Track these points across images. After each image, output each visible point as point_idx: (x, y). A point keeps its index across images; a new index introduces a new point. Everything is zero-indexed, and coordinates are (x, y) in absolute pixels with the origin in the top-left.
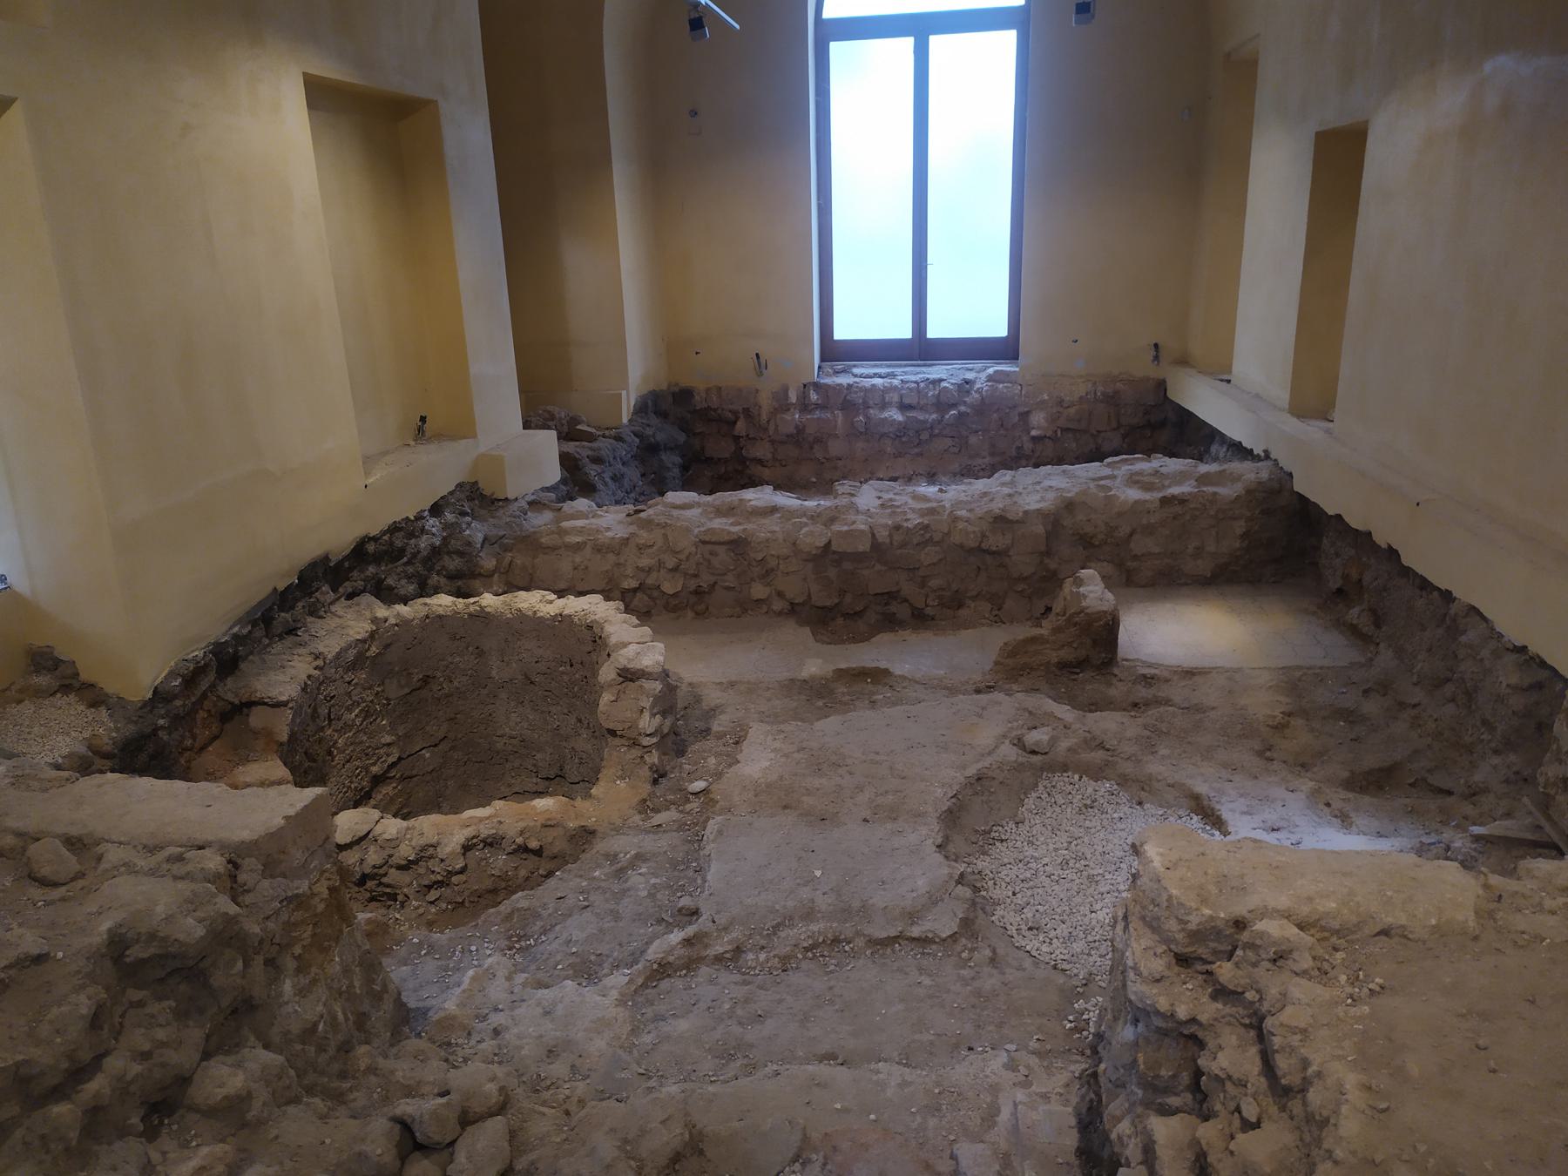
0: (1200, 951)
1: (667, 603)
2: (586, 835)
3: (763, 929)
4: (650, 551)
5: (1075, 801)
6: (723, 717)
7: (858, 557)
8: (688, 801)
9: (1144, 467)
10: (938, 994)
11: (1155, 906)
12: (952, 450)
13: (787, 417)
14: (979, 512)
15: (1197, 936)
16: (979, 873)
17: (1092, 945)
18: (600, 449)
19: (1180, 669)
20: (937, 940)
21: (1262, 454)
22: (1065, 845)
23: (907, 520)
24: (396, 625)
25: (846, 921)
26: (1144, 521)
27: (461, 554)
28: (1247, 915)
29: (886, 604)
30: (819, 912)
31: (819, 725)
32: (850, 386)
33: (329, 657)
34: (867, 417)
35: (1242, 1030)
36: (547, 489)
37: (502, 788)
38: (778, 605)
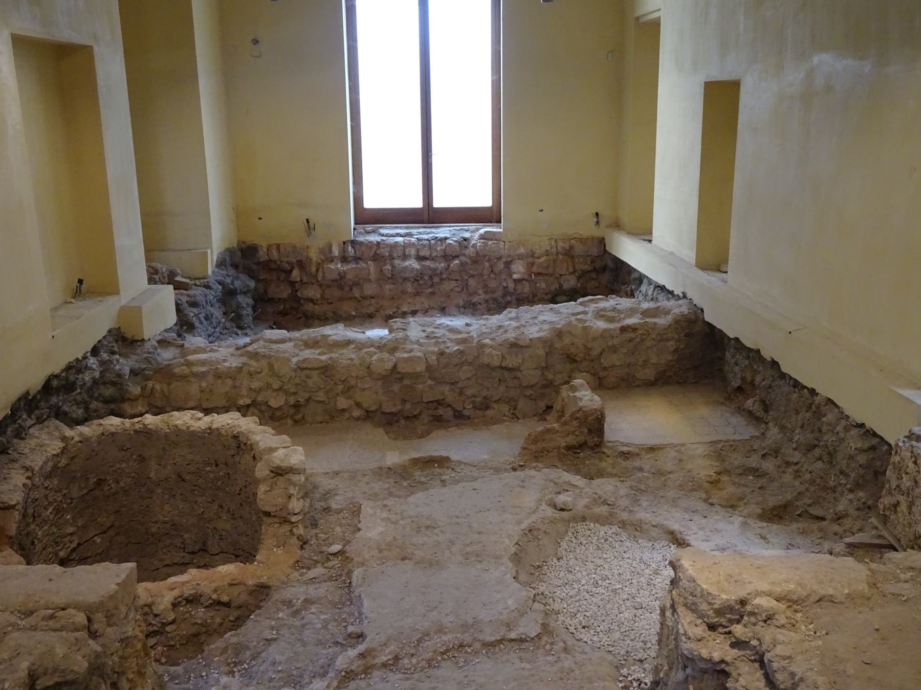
0: (721, 620)
1: (273, 414)
2: (262, 590)
3: (411, 642)
4: (260, 376)
5: (593, 541)
6: (338, 498)
7: (416, 376)
8: (328, 560)
9: (606, 306)
10: (536, 673)
11: (693, 597)
12: (457, 289)
13: (332, 266)
14: (500, 340)
15: (719, 612)
16: (542, 593)
17: (624, 634)
18: (195, 296)
19: (645, 447)
20: (528, 639)
21: (681, 295)
22: (593, 571)
23: (448, 347)
24: (80, 442)
25: (464, 632)
26: (610, 344)
27: (113, 384)
28: (748, 597)
29: (435, 409)
30: (446, 628)
31: (411, 499)
32: (378, 243)
33: (37, 468)
34: (393, 266)
35: (750, 663)
36: (166, 331)
37: (156, 562)
38: (357, 413)
